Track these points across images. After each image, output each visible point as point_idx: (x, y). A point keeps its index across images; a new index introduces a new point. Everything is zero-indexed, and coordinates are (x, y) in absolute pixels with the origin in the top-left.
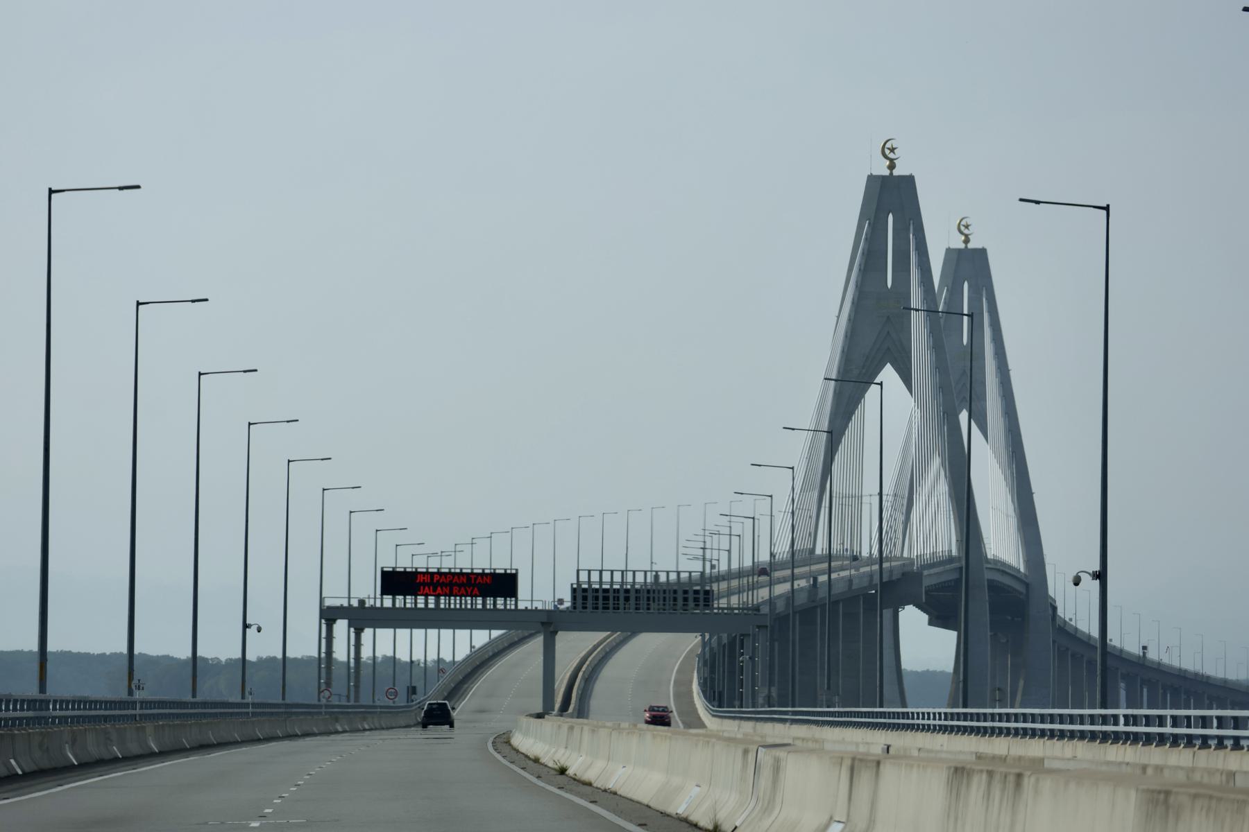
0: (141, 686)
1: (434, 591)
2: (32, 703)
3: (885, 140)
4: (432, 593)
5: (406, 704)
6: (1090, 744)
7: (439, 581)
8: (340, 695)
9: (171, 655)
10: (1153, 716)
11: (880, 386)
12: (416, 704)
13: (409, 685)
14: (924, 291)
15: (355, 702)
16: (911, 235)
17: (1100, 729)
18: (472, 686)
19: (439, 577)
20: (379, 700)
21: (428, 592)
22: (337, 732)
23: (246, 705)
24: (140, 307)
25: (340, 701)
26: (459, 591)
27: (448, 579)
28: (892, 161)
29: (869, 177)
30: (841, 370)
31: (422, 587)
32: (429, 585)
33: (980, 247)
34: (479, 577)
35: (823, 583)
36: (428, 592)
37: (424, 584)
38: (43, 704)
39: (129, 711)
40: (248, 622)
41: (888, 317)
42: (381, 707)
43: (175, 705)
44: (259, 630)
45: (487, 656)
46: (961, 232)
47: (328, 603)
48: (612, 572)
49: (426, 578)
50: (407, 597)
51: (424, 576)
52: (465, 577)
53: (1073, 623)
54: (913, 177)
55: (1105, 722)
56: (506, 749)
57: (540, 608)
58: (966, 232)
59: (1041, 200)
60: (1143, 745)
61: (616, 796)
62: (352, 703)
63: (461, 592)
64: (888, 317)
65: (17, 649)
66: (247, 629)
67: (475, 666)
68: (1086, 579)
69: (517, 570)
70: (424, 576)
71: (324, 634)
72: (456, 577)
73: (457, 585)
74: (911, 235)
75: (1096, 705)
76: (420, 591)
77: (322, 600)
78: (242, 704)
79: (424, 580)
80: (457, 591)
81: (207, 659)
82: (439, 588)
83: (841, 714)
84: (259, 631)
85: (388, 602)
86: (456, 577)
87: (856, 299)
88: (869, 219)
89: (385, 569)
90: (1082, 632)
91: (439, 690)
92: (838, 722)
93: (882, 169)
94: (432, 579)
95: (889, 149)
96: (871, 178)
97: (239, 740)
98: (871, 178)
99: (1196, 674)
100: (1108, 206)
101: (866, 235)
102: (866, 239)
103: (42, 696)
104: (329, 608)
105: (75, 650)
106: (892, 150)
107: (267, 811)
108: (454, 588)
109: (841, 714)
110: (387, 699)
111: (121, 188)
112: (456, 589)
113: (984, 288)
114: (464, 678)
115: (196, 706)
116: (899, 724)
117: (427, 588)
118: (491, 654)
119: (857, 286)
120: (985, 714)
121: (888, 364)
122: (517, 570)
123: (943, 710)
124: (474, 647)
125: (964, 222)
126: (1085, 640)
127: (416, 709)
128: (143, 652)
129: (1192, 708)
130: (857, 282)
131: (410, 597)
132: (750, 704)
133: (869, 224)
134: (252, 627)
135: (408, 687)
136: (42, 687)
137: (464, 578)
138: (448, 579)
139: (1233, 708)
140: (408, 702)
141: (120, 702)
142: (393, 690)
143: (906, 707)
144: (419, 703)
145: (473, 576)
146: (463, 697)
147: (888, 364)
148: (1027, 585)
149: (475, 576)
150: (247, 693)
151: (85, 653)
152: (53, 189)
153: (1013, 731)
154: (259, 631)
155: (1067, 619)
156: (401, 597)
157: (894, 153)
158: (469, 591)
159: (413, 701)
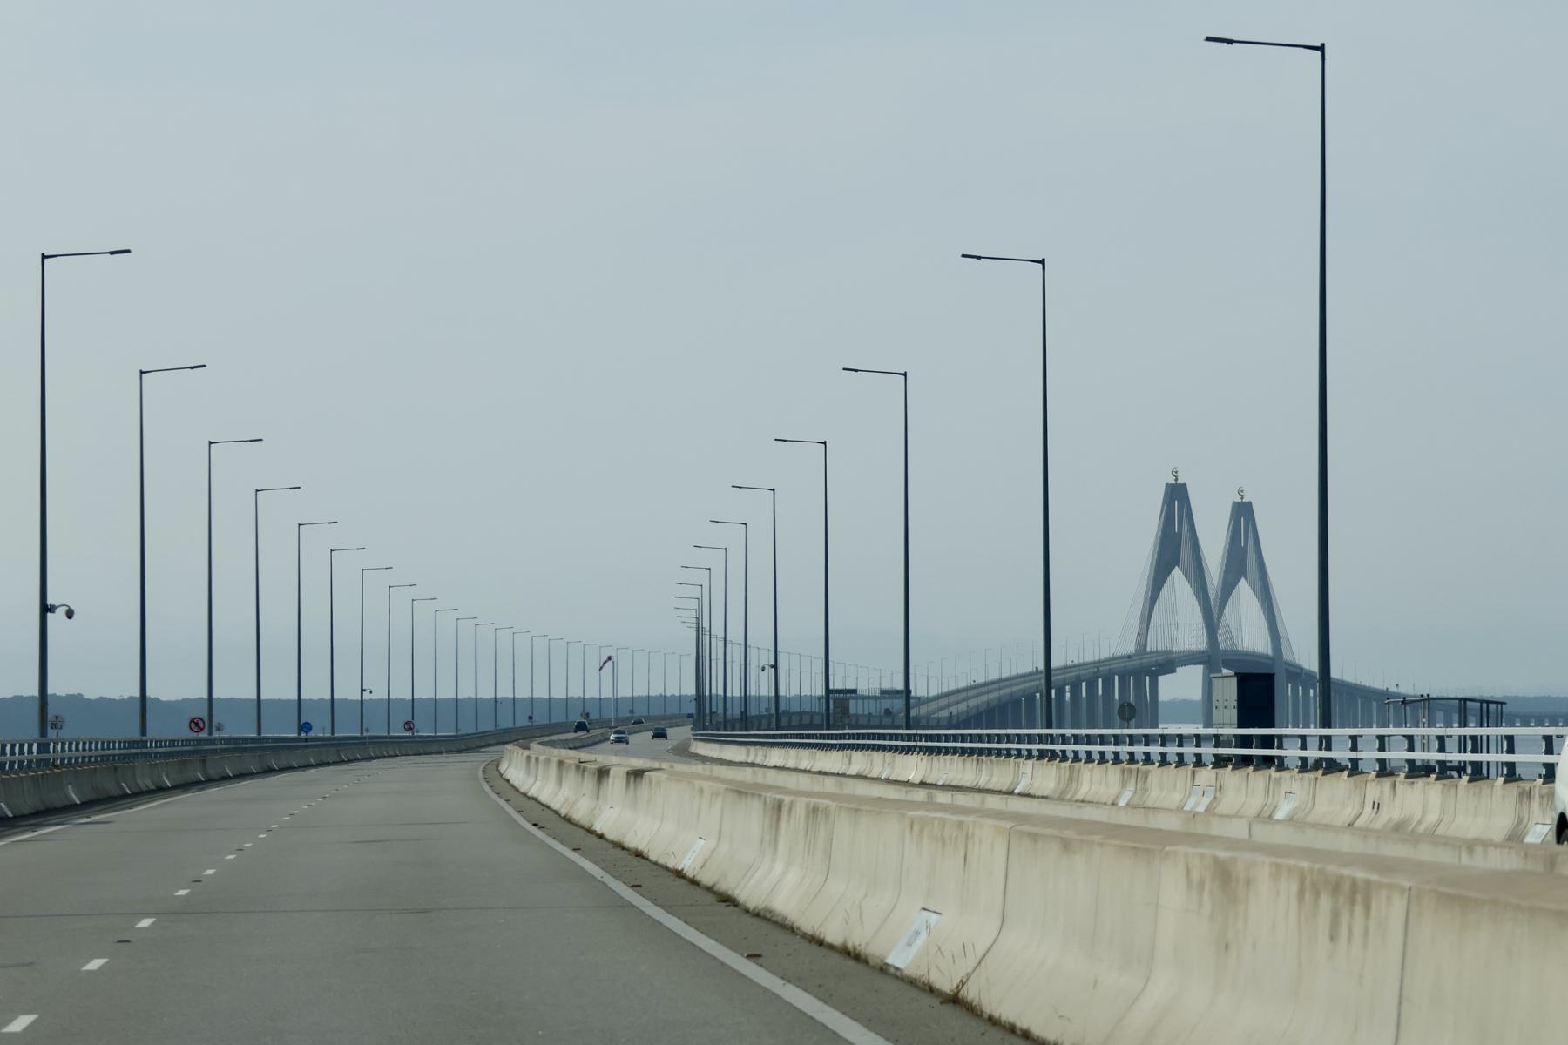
0: (59, 724)
10: (958, 735)
11: (1041, 265)
23: (365, 738)
24: (46, 260)
40: (50, 602)
44: (70, 614)
59: (983, 256)
60: (1233, 769)
61: (601, 840)
66: (49, 614)
83: (712, 735)
84: (763, 670)
93: (1238, 499)
96: (1234, 503)
97: (231, 775)
98: (1234, 503)
100: (1323, 45)
103: (210, 737)
105: (91, 694)
107: (287, 818)
111: (112, 253)
115: (136, 746)
128: (104, 696)
132: (1084, 720)
134: (57, 611)
136: (143, 731)
139: (986, 728)
141: (134, 742)
143: (1272, 726)
150: (214, 729)
151: (69, 696)
152: (46, 254)
153: (1025, 753)
154: (763, 670)
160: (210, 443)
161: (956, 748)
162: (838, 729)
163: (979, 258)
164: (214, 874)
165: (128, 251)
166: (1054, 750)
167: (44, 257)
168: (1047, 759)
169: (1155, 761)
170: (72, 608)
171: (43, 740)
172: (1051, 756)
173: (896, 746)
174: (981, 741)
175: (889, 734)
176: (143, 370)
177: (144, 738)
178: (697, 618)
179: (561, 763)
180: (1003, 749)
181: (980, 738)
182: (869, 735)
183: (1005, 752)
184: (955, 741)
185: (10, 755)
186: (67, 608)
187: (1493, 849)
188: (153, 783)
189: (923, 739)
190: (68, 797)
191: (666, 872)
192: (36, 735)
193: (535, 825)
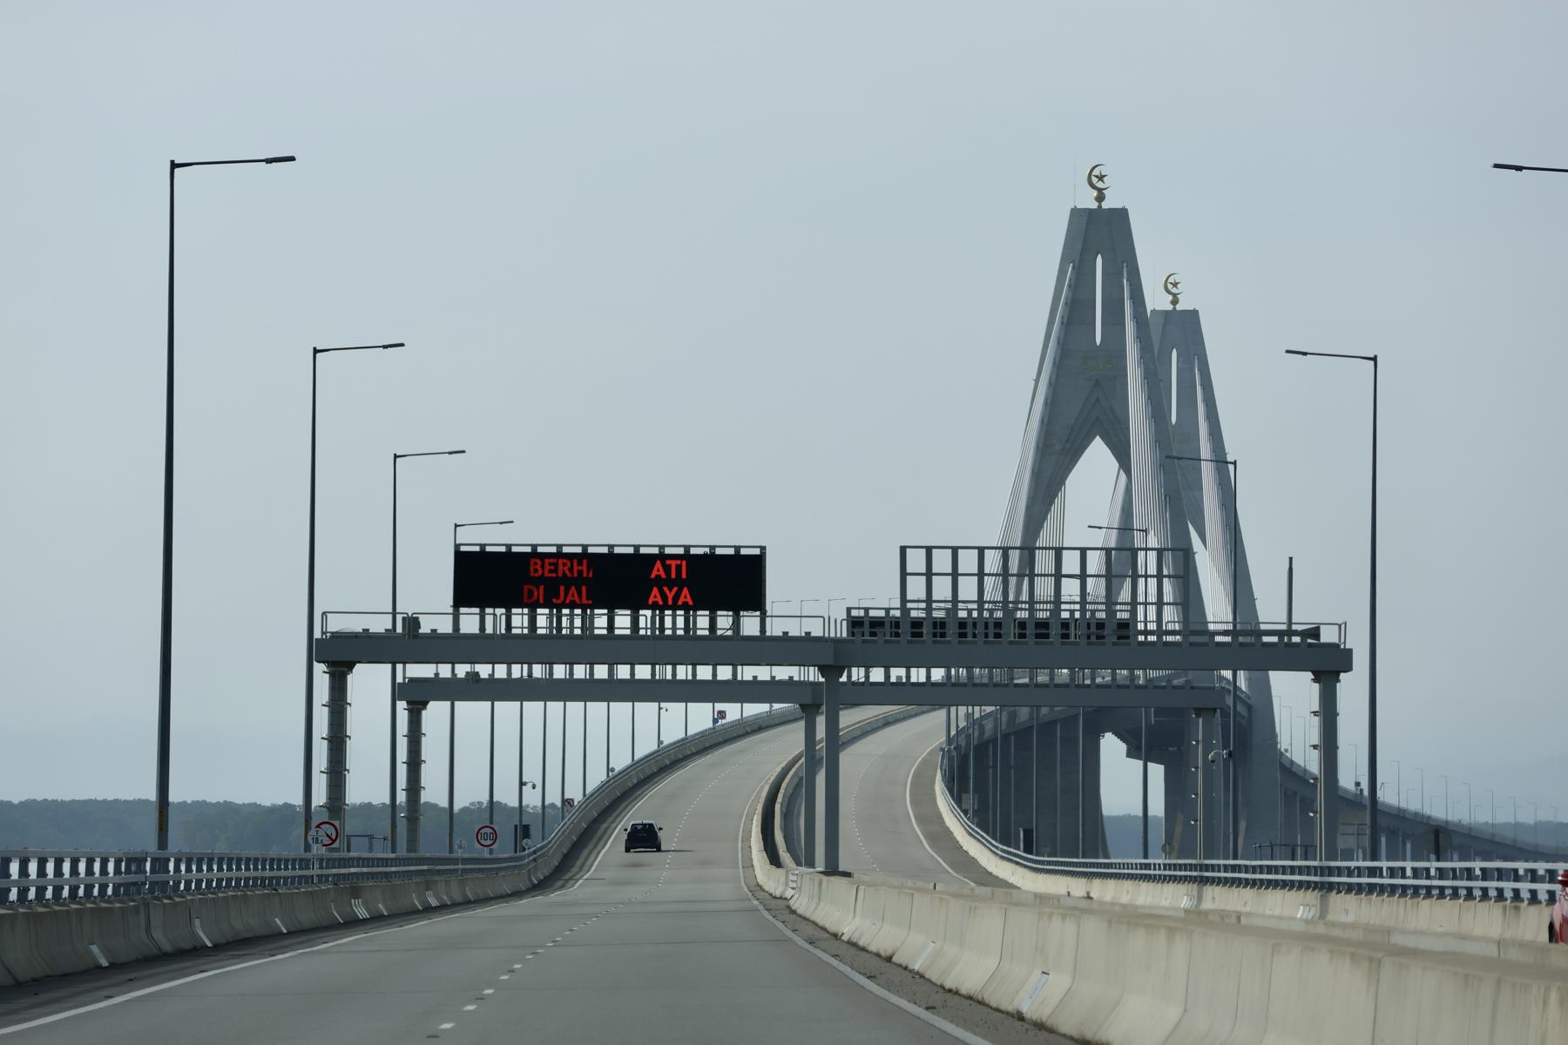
2: (331, 862)
3: (1092, 166)
5: (513, 854)
6: (1274, 891)
8: (371, 837)
9: (258, 803)
12: (529, 855)
13: (518, 823)
14: (1141, 348)
15: (409, 850)
16: (1125, 281)
18: (614, 825)
20: (460, 847)
22: (353, 923)
23: (455, 861)
25: (371, 850)
28: (1100, 190)
29: (1072, 209)
30: (1041, 446)
33: (1119, 206)
35: (1087, 679)
36: (576, 598)
38: (324, 863)
40: (524, 780)
41: (1098, 380)
42: (465, 861)
45: (630, 785)
46: (1169, 292)
48: (955, 550)
50: (514, 611)
51: (580, 564)
53: (1288, 755)
54: (1127, 210)
55: (1350, 874)
57: (817, 632)
58: (1174, 290)
62: (402, 851)
64: (1098, 380)
65: (90, 798)
67: (613, 798)
69: (763, 548)
70: (580, 564)
74: (1125, 281)
76: (558, 598)
78: (450, 859)
79: (580, 572)
81: (294, 806)
83: (1049, 863)
85: (470, 622)
87: (1058, 358)
88: (1073, 262)
89: (463, 549)
90: (1297, 765)
91: (565, 831)
92: (1105, 873)
93: (1088, 201)
95: (1096, 176)
96: (1076, 213)
98: (1076, 213)
99: (1416, 814)
100: (1376, 356)
101: (1070, 280)
102: (1069, 286)
106: (1101, 178)
109: (1049, 863)
110: (477, 845)
113: (1196, 357)
114: (599, 815)
117: (573, 590)
118: (635, 781)
119: (1058, 343)
121: (1098, 437)
122: (763, 548)
123: (1160, 861)
124: (613, 770)
125: (1171, 280)
126: (1301, 774)
127: (529, 863)
128: (229, 800)
130: (1059, 338)
131: (519, 611)
133: (1074, 268)
135: (516, 826)
140: (516, 852)
142: (488, 831)
144: (535, 852)
146: (602, 843)
147: (1098, 437)
148: (1249, 708)
152: (318, 348)
154: (534, 788)
155: (1283, 750)
156: (500, 611)
157: (1103, 182)
158: (670, 596)
159: (524, 849)
160: (174, 166)
161: (1394, 885)
164: (441, 1024)
165: (402, 345)
167: (396, 457)
169: (1543, 900)
171: (161, 854)
173: (1292, 882)
175: (1268, 866)
176: (398, 454)
177: (308, 855)
180: (1448, 887)
183: (1450, 891)
184: (1246, 872)
185: (101, 875)
188: (108, 961)
190: (195, 935)
191: (879, 959)
192: (151, 845)
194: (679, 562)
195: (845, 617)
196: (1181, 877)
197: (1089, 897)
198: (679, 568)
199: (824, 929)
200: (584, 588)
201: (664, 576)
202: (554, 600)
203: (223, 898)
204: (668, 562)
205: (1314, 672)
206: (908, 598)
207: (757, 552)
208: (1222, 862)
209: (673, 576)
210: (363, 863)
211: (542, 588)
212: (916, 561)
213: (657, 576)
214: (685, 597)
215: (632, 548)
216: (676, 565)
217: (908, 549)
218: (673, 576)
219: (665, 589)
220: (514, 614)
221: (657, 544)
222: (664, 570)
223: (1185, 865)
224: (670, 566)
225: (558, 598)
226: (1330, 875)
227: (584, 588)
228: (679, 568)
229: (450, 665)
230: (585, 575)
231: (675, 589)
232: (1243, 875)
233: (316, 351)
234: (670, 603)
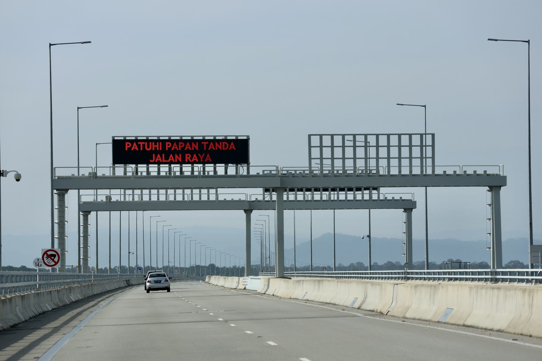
1: (167, 158)
4: (164, 161)
7: (170, 149)
17: (494, 277)
19: (170, 144)
21: (160, 160)
26: (191, 158)
27: (180, 147)
31: (154, 155)
32: (161, 153)
34: (212, 144)
36: (160, 160)
37: (156, 152)
38: (18, 278)
39: (3, 284)
43: (22, 278)
47: (59, 173)
49: (157, 146)
51: (156, 144)
52: (197, 143)
55: (371, 274)
56: (210, 284)
62: (276, 275)
63: (193, 159)
68: (365, 237)
70: (156, 144)
71: (56, 206)
72: (188, 144)
73: (188, 151)
75: (425, 268)
76: (152, 160)
77: (53, 170)
79: (156, 148)
80: (189, 158)
82: (171, 156)
85: (120, 171)
86: (188, 144)
89: (116, 138)
94: (164, 146)
104: (59, 178)
108: (187, 155)
112: (188, 156)
116: (318, 276)
117: (159, 156)
120: (347, 273)
122: (248, 136)
129: (540, 268)
132: (294, 271)
134: (8, 175)
137: (196, 144)
138: (180, 147)
139: (352, 271)
145: (205, 143)
149: (207, 143)
158: (201, 158)
160: (78, 108)
161: (376, 277)
162: (446, 269)
163: (403, 105)
166: (528, 279)
168: (400, 280)
170: (20, 173)
172: (429, 280)
174: (353, 274)
178: (261, 237)
179: (338, 282)
181: (379, 274)
182: (341, 273)
185: (493, 269)
186: (16, 173)
187: (259, 291)
189: (426, 273)
193: (343, 310)
194: (144, 143)
195: (387, 166)
196: (327, 276)
197: (245, 289)
198: (144, 145)
199: (323, 303)
200: (163, 155)
201: (137, 149)
202: (151, 161)
203: (27, 295)
204: (139, 143)
205: (489, 187)
206: (380, 157)
207: (245, 138)
208: (326, 272)
209: (141, 149)
210: (28, 279)
211: (180, 155)
212: (315, 141)
213: (187, 149)
214: (171, 158)
215: (190, 137)
216: (143, 144)
217: (391, 136)
218: (141, 149)
219: (199, 155)
220: (195, 166)
221: (145, 136)
222: (138, 147)
223: (321, 273)
224: (140, 145)
225: (152, 160)
226: (496, 275)
227: (163, 155)
228: (144, 145)
229: (77, 190)
230: (158, 149)
231: (204, 155)
232: (325, 275)
233: (50, 45)
234: (201, 161)
